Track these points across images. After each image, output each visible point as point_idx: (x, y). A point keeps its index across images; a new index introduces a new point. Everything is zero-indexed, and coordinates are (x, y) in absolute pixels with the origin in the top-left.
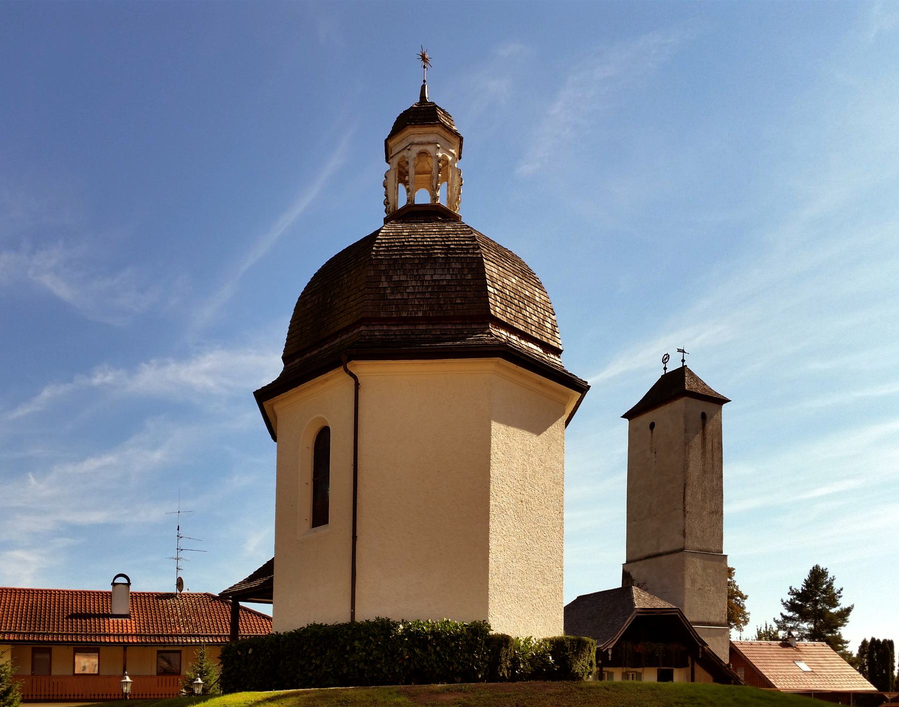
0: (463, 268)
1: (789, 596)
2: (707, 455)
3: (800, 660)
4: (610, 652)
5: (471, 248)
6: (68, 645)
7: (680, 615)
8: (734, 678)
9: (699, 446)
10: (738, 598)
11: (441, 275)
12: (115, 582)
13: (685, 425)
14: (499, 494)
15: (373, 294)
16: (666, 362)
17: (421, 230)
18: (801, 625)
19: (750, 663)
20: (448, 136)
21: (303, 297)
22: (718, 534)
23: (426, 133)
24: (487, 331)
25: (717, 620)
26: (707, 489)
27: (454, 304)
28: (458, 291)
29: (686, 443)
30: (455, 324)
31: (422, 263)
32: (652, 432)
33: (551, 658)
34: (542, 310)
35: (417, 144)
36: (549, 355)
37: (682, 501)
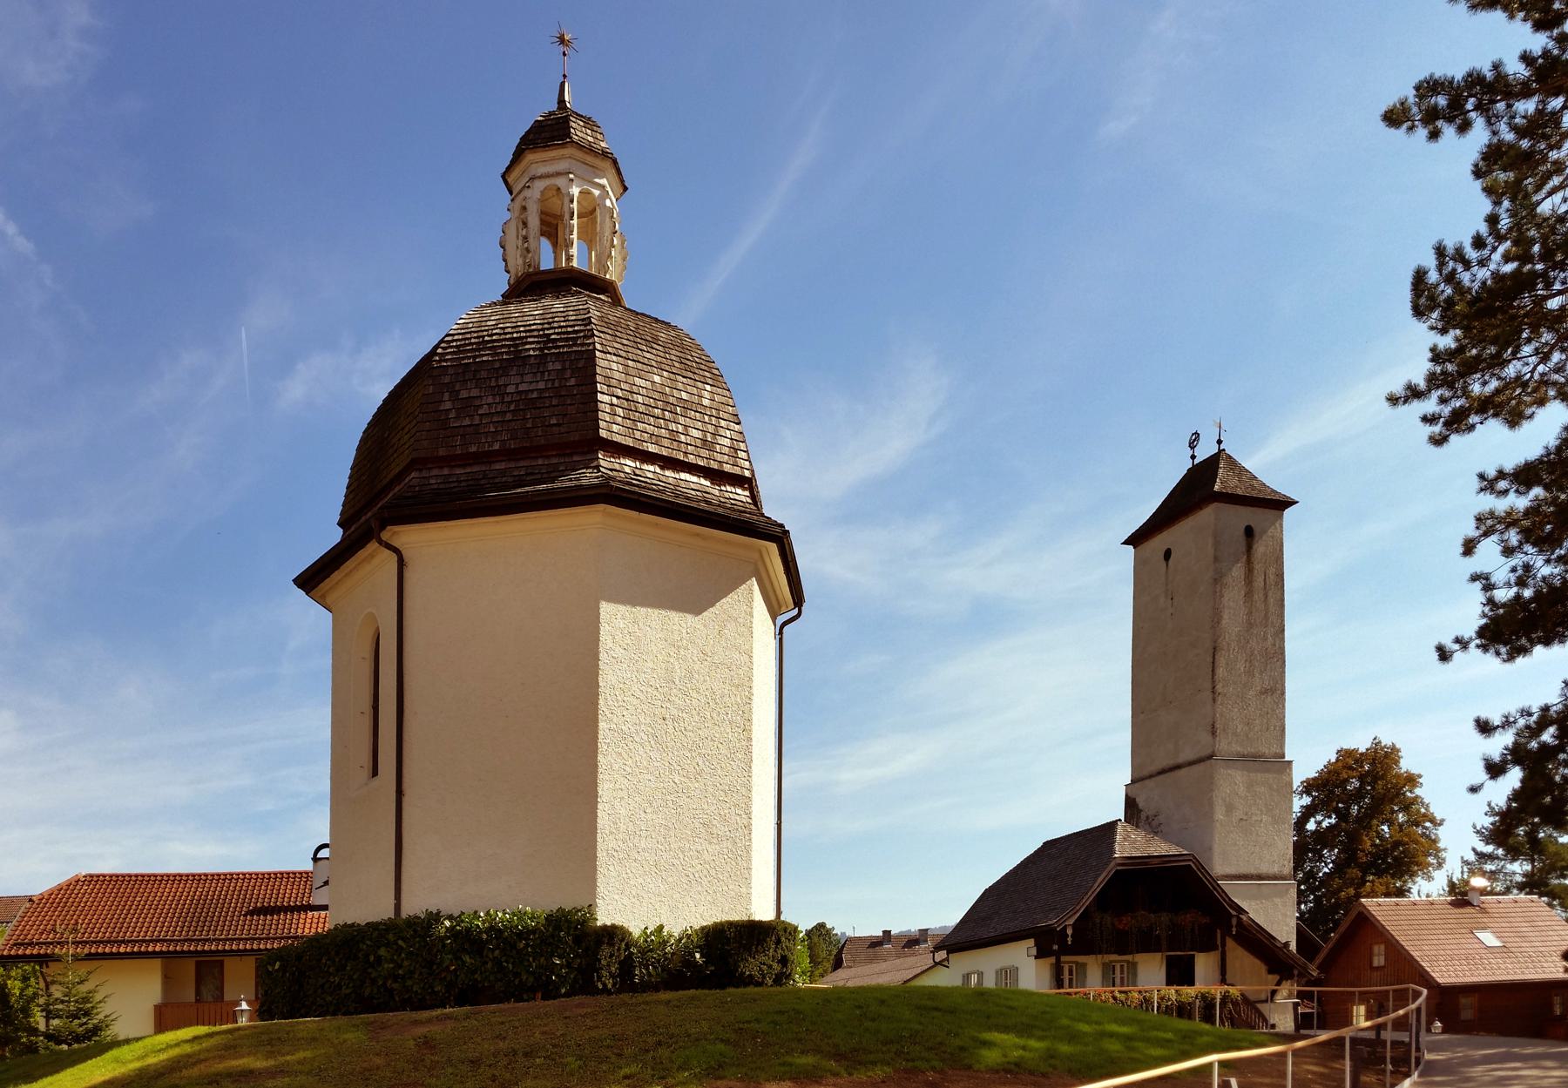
0: (564, 369)
1: (1487, 817)
2: (1256, 596)
3: (1484, 928)
4: (1069, 932)
5: (580, 337)
6: (239, 955)
8: (1299, 965)
9: (1241, 582)
10: (1428, 824)
11: (531, 382)
12: (318, 856)
13: (1215, 550)
14: (618, 711)
15: (429, 421)
18: (1508, 866)
19: (1390, 936)
20: (590, 159)
22: (1275, 727)
23: (553, 159)
24: (595, 464)
25: (1275, 869)
26: (1256, 652)
27: (547, 426)
28: (554, 406)
29: (1215, 580)
30: (548, 457)
31: (505, 367)
32: (1167, 565)
33: (698, 955)
35: (541, 177)
36: (723, 488)
37: (1211, 677)
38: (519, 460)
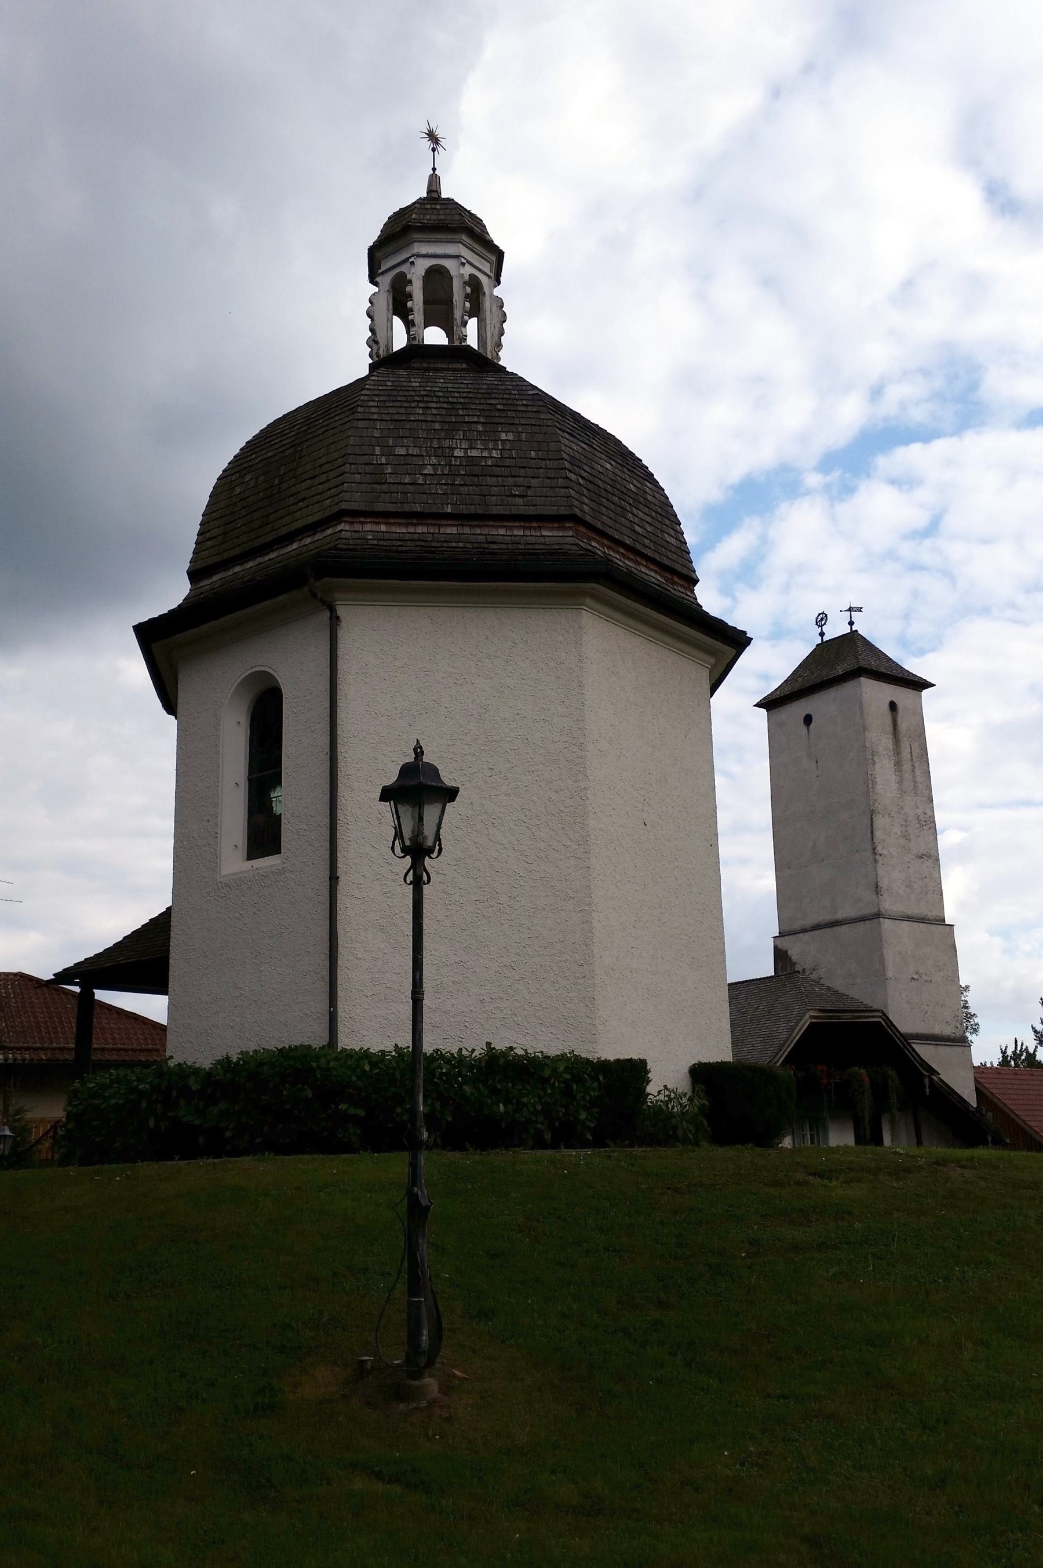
7: (886, 1023)
16: (822, 625)
17: (442, 381)
21: (224, 478)
34: (659, 516)
38: (324, 530)
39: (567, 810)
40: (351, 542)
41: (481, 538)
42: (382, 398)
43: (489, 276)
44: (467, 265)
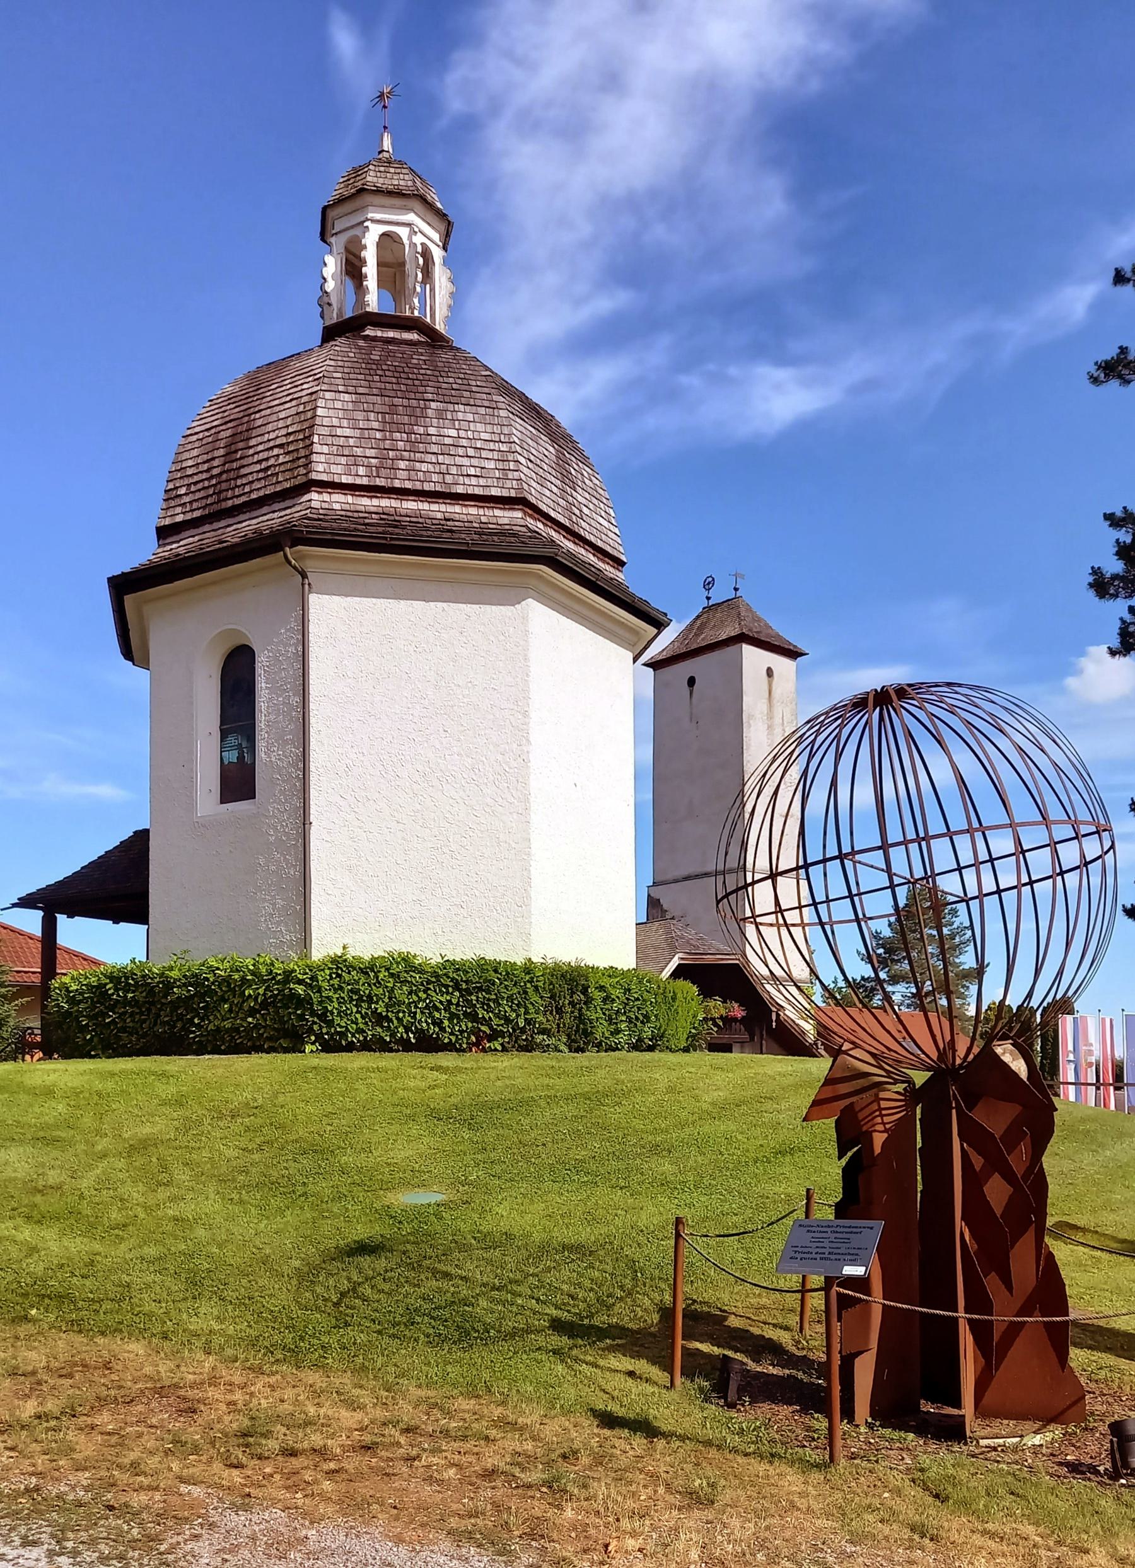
39: (511, 771)
40: (321, 511)
41: (439, 515)
42: (346, 370)
43: (438, 246)
44: (419, 234)
